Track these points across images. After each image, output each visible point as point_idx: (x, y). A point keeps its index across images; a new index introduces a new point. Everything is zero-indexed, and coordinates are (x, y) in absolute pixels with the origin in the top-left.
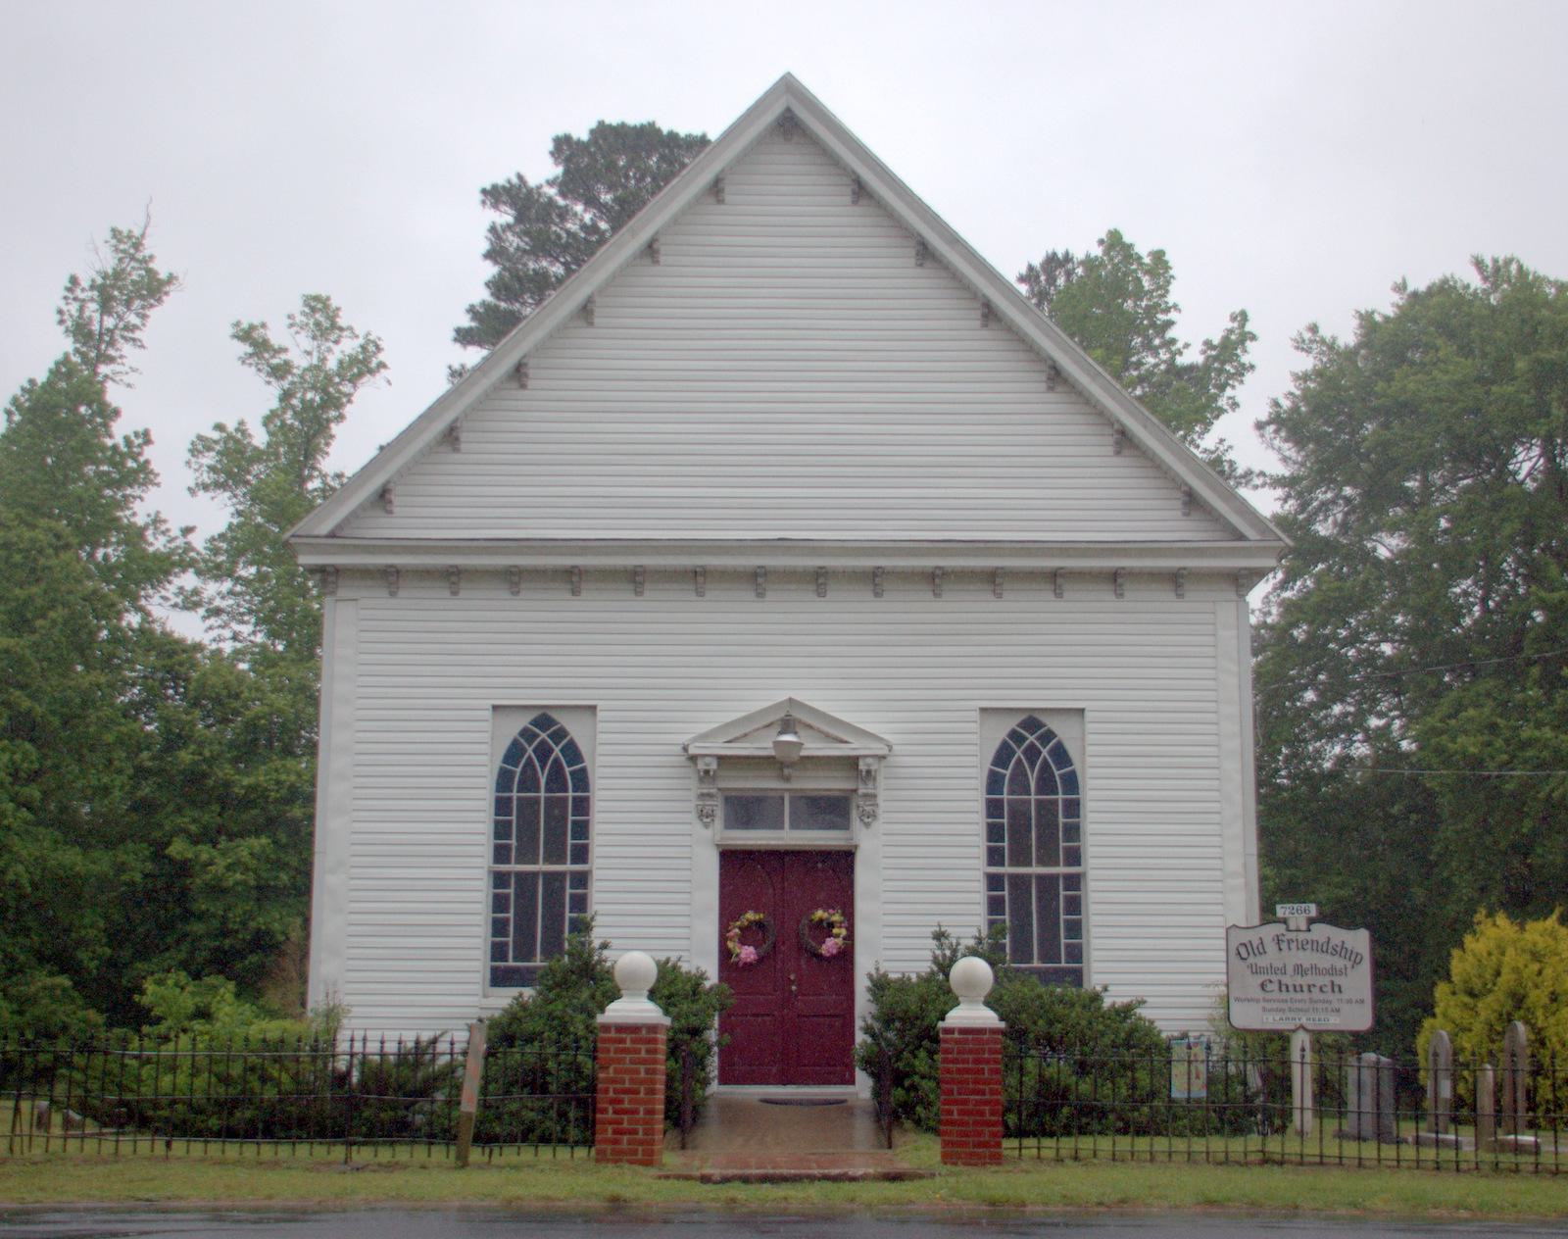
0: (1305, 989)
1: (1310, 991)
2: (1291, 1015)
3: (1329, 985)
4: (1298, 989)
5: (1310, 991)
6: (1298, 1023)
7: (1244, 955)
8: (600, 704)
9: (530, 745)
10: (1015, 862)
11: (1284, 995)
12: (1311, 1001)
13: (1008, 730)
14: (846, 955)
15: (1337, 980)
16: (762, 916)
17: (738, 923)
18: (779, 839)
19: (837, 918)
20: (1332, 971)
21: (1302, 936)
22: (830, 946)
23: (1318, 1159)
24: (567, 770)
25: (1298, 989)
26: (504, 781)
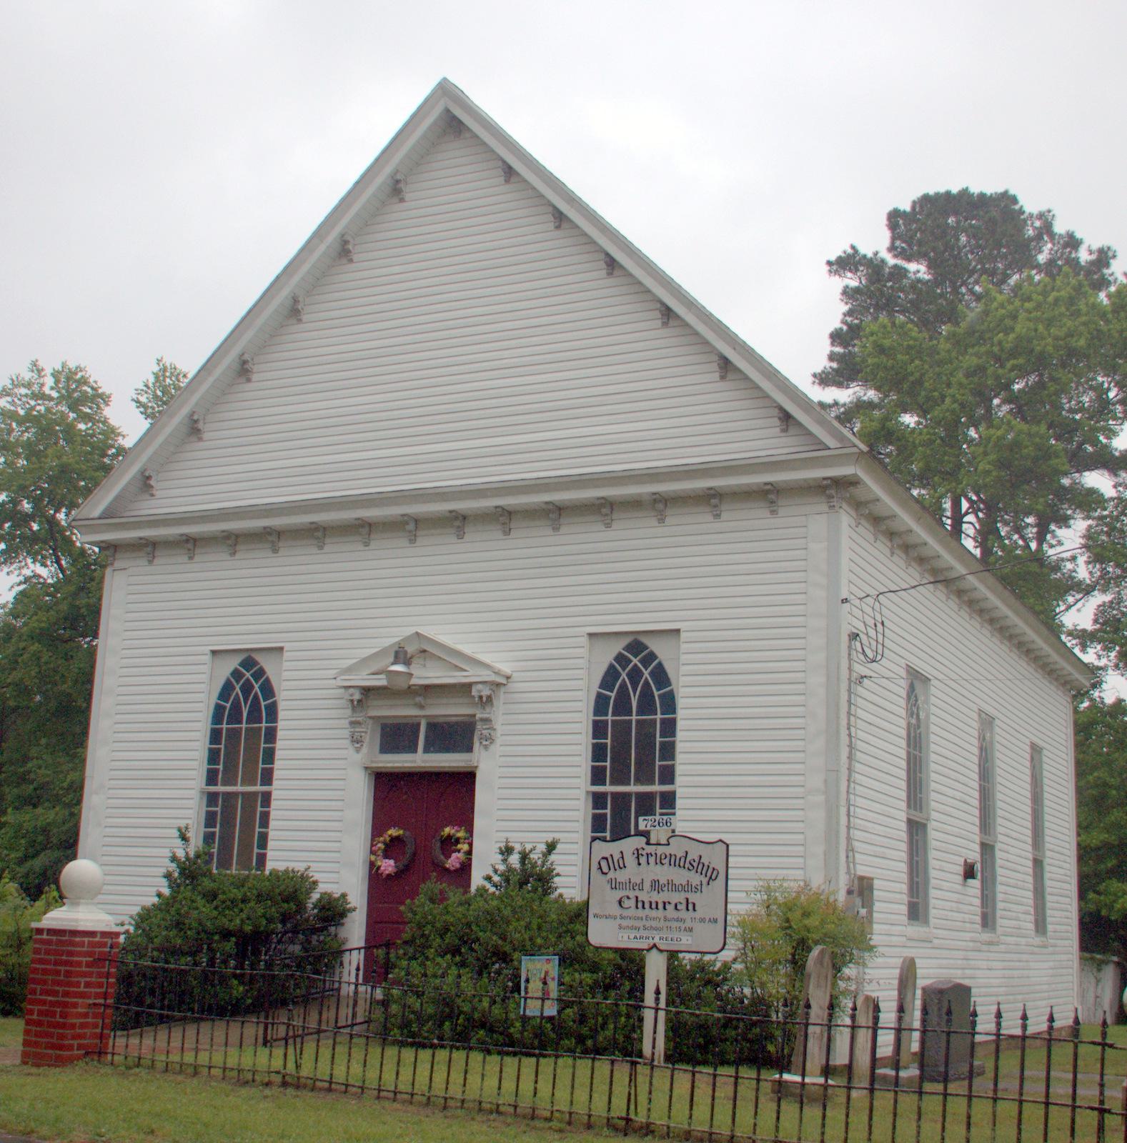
0: (660, 906)
1: (665, 908)
2: (645, 934)
3: (684, 902)
4: (654, 906)
5: (665, 908)
6: (651, 942)
7: (605, 869)
8: (287, 646)
9: (238, 683)
10: (615, 782)
11: (640, 913)
12: (666, 919)
13: (614, 654)
14: (466, 868)
15: (693, 897)
16: (401, 832)
17: (381, 839)
18: (412, 762)
19: (461, 834)
20: (688, 887)
21: (660, 850)
22: (453, 861)
23: (326, 1085)
24: (263, 704)
25: (654, 906)
26: (601, 704)
